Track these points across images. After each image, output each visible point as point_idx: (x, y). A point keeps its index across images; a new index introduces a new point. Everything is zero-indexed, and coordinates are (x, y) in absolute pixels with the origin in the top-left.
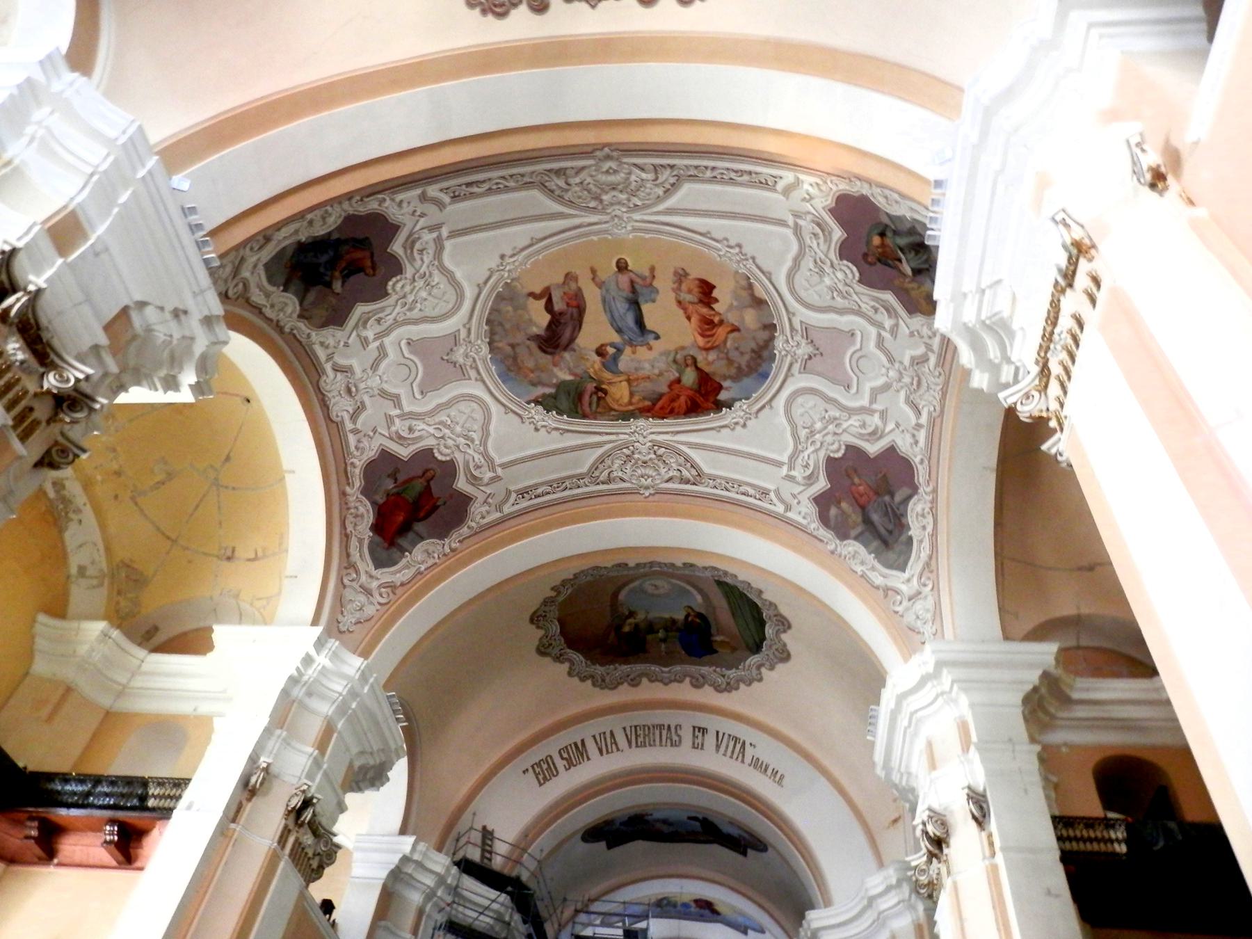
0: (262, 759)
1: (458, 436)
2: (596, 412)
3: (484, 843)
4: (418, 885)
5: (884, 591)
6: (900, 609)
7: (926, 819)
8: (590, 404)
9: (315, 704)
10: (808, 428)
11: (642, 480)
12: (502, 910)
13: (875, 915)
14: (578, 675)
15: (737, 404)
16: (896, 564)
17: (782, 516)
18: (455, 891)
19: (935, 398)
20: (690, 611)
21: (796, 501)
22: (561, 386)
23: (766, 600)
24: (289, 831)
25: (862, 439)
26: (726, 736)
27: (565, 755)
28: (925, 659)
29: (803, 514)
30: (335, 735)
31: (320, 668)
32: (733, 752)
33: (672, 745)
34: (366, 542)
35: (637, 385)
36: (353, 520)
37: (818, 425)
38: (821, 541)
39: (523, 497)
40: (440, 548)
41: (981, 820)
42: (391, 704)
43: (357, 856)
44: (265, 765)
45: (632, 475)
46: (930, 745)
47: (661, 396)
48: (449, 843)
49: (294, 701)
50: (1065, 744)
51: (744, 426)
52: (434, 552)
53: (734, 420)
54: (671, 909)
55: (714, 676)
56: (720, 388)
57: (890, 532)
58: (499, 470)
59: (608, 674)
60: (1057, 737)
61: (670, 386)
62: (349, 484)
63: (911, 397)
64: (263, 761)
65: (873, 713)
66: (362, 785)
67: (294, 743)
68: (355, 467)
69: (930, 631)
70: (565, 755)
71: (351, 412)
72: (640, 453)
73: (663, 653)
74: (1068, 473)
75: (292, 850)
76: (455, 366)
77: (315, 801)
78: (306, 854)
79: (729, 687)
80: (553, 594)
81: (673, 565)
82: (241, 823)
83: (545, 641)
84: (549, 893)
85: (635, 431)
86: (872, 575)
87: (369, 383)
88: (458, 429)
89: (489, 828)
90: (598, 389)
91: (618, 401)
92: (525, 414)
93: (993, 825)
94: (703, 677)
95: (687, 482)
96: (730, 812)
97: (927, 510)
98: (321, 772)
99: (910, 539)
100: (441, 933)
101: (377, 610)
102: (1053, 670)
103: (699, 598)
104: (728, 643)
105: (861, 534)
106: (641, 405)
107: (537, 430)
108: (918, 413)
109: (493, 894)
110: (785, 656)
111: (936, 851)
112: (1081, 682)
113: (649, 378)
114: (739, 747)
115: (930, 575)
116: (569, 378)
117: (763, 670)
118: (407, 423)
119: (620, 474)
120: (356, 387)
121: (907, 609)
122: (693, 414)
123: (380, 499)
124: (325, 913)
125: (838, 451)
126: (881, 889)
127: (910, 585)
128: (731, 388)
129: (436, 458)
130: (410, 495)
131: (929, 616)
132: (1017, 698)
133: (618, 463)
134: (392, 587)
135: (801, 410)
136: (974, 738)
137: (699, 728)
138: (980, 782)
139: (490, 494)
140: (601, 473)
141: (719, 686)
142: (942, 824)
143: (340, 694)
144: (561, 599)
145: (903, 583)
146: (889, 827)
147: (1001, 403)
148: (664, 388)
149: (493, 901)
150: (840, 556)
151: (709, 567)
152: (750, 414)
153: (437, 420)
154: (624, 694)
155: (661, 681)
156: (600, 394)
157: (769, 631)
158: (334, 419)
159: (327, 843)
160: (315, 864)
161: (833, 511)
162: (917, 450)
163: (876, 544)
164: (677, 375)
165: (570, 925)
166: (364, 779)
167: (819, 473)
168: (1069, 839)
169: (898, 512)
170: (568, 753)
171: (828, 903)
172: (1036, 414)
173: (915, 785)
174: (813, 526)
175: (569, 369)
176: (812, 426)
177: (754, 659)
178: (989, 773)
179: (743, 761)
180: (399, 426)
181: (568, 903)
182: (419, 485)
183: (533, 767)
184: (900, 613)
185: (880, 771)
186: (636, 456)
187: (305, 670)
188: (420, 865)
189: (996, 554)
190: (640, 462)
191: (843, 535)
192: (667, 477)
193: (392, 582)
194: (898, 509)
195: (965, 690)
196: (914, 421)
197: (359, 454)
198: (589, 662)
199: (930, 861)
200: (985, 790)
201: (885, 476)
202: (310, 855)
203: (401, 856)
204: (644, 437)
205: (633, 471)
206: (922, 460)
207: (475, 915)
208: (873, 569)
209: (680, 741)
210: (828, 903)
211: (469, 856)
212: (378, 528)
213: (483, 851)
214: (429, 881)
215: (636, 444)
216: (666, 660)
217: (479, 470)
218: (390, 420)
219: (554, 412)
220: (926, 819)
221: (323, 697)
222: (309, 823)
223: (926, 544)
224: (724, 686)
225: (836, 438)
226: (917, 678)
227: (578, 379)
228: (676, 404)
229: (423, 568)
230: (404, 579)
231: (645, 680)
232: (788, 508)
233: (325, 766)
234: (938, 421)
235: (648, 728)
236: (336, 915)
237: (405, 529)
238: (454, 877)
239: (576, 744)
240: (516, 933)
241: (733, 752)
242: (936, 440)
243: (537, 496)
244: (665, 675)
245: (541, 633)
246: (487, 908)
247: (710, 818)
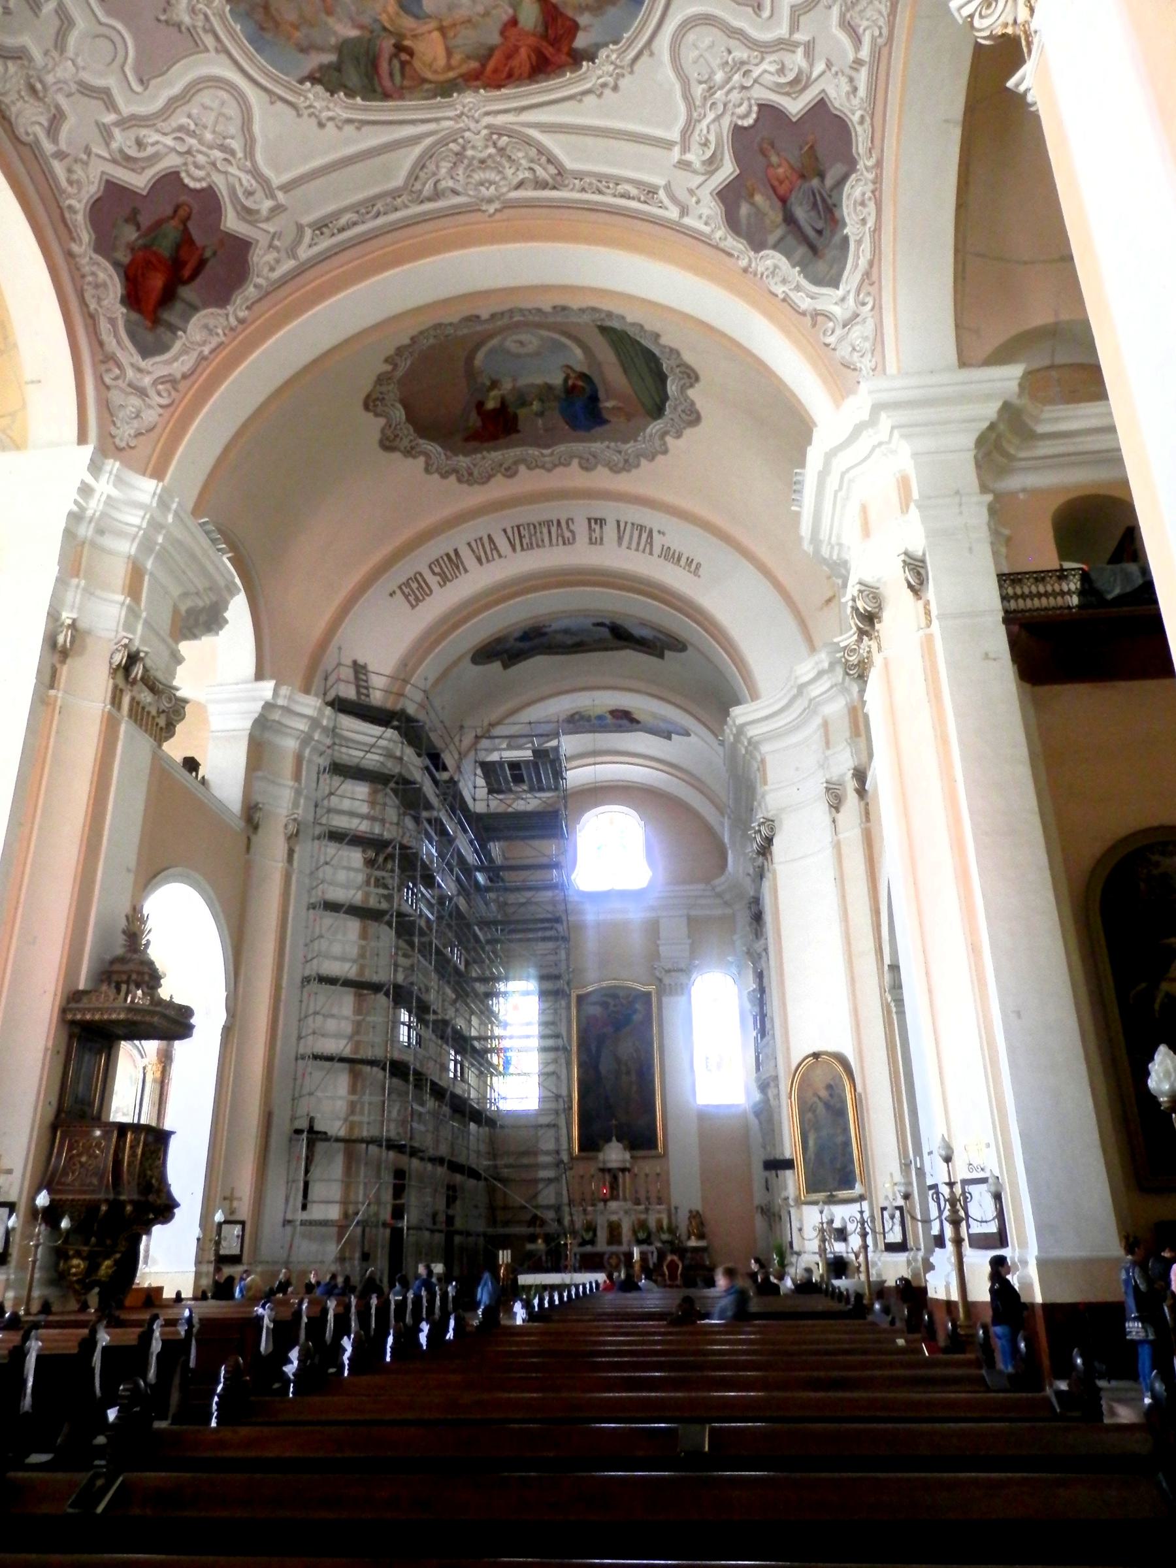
0: (64, 615)
1: (211, 147)
2: (402, 88)
3: (357, 678)
4: (289, 731)
5: (812, 318)
6: (831, 340)
7: (856, 594)
8: (391, 75)
9: (108, 542)
10: (705, 82)
11: (483, 189)
12: (391, 745)
13: (806, 704)
14: (438, 471)
15: (603, 53)
16: (828, 277)
17: (678, 223)
18: (333, 732)
19: (880, 13)
20: (569, 371)
21: (694, 199)
22: (343, 47)
23: (665, 347)
24: (121, 691)
25: (779, 93)
26: (629, 527)
27: (437, 570)
28: (859, 404)
29: (704, 218)
30: (147, 578)
31: (104, 498)
32: (638, 544)
33: (564, 544)
34: (121, 324)
35: (455, 36)
36: (93, 292)
37: (719, 76)
38: (730, 255)
39: (322, 234)
40: (222, 320)
41: (917, 588)
42: (207, 533)
43: (211, 708)
44: (69, 622)
45: (468, 183)
46: (864, 510)
47: (492, 50)
48: (318, 681)
49: (84, 543)
50: (1024, 490)
51: (615, 88)
52: (216, 327)
53: (601, 81)
54: (586, 723)
55: (608, 453)
56: (574, 28)
57: (820, 232)
58: (280, 195)
59: (475, 465)
60: (1013, 482)
61: (502, 33)
62: (73, 239)
63: (848, 16)
64: (67, 616)
65: (799, 478)
66: (196, 631)
67: (98, 592)
68: (75, 212)
69: (869, 365)
70: (437, 570)
71: (46, 124)
72: (474, 147)
73: (541, 432)
74: (1036, 117)
75: (131, 710)
76: (180, 31)
77: (142, 655)
78: (149, 713)
79: (628, 465)
80: (389, 368)
81: (539, 310)
82: (62, 685)
83: (389, 432)
84: (442, 722)
85: (462, 114)
86: (796, 297)
87: (60, 73)
88: (208, 136)
89: (361, 661)
90: (399, 48)
91: (430, 66)
92: (300, 101)
93: (931, 593)
94: (594, 456)
95: (544, 185)
96: (646, 615)
97: (869, 194)
98: (141, 622)
99: (846, 239)
100: (327, 776)
101: (160, 415)
102: (1016, 401)
103: (578, 352)
104: (619, 409)
105: (782, 239)
106: (464, 69)
107: (321, 125)
108: (857, 40)
109: (377, 730)
110: (694, 418)
111: (867, 628)
112: (1050, 412)
113: (469, 21)
114: (644, 537)
115: (870, 289)
116: (354, 33)
117: (668, 439)
118: (132, 134)
119: (450, 183)
120: (41, 81)
121: (841, 339)
122: (541, 76)
123: (125, 257)
124: (190, 771)
125: (746, 116)
126: (811, 675)
127: (845, 306)
128: (591, 26)
129: (186, 186)
130: (165, 247)
131: (867, 345)
132: (967, 441)
133: (445, 167)
134: (171, 381)
135: (694, 54)
136: (916, 495)
137: (596, 520)
138: (918, 546)
139: (275, 234)
140: (424, 184)
141: (616, 465)
142: (874, 598)
143: (140, 528)
144: (399, 373)
145: (836, 303)
146: (822, 609)
147: (952, 14)
148: (495, 39)
149: (380, 737)
150: (755, 275)
151: (588, 308)
152: (622, 67)
153: (174, 125)
154: (499, 488)
155: (543, 467)
156: (404, 57)
157: (672, 388)
158: (24, 138)
159: (170, 699)
160: (162, 721)
161: (744, 209)
162: (856, 102)
163: (802, 250)
164: (511, 11)
165: (473, 753)
166: (197, 624)
167: (722, 154)
168: (1016, 597)
169: (830, 201)
170: (441, 568)
171: (755, 696)
172: (999, 31)
173: (847, 557)
174: (719, 234)
175: (352, 19)
176: (710, 78)
177: (655, 427)
178: (931, 534)
179: (651, 553)
180: (121, 140)
181: (466, 730)
182: (172, 232)
183: (400, 588)
184: (832, 346)
185: (807, 546)
186: (470, 153)
187: (87, 503)
188: (287, 710)
189: (957, 251)
190: (475, 162)
191: (758, 245)
192: (515, 181)
193: (170, 375)
194: (830, 196)
195: (904, 436)
196: (851, 56)
197: (75, 191)
198: (449, 453)
199: (860, 640)
200: (924, 555)
201: (812, 147)
202: (154, 712)
203: (262, 703)
204: (477, 122)
205: (469, 176)
206: (862, 117)
207: (361, 754)
208: (798, 288)
209: (574, 538)
210: (755, 696)
211: (343, 694)
212: (133, 298)
213: (358, 687)
214: (302, 726)
215: (467, 134)
216: (545, 440)
217: (251, 199)
218: (105, 132)
219: (342, 94)
220: (856, 594)
221: (120, 534)
222: (142, 679)
223: (866, 245)
224: (621, 465)
225: (744, 94)
226: (850, 429)
227: (367, 35)
228: (515, 63)
229: (206, 350)
230: (186, 368)
231: (522, 468)
232: (684, 211)
233: (144, 615)
234: (885, 51)
235: (534, 527)
236: (202, 772)
237: (168, 297)
238: (329, 718)
239: (448, 555)
240: (412, 768)
241: (638, 544)
242: (881, 85)
243: (342, 230)
244: (547, 459)
245: (382, 421)
246: (373, 746)
247: (619, 622)
